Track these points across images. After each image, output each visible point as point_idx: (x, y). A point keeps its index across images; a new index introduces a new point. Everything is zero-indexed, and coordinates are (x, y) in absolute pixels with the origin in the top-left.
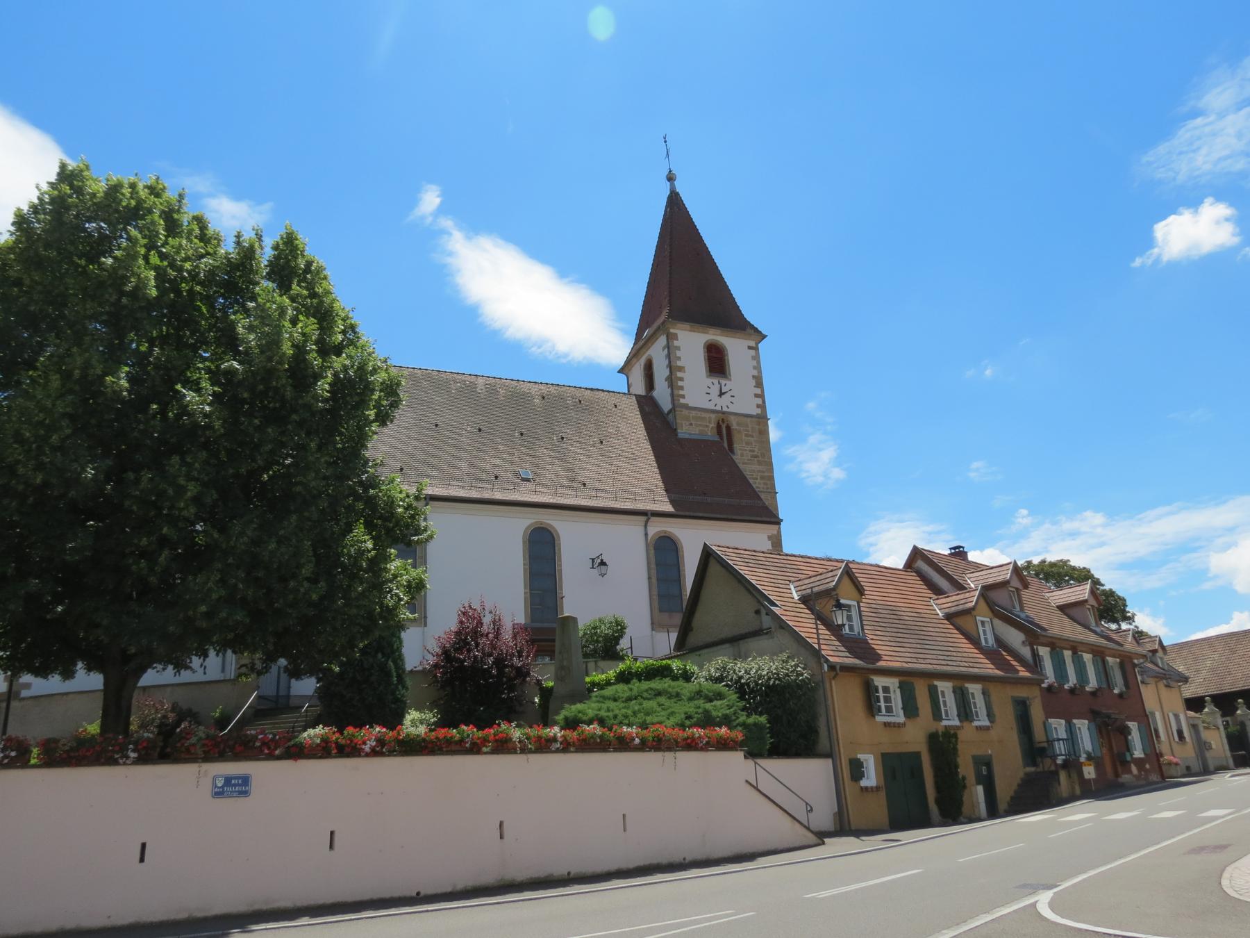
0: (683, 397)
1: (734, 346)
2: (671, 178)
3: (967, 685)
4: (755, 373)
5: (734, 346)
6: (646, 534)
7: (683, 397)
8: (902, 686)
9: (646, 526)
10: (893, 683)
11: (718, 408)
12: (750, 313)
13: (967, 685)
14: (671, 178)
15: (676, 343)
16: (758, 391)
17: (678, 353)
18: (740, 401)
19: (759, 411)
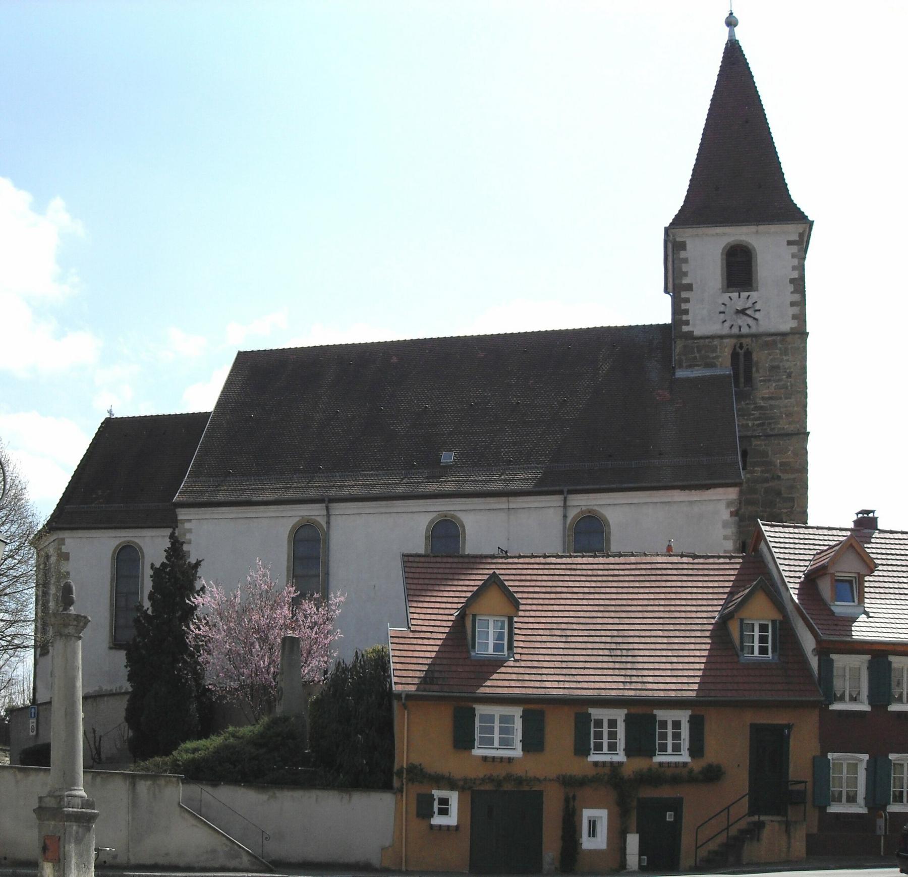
0: (687, 323)
1: (766, 243)
2: (731, 22)
3: (655, 712)
4: (795, 275)
5: (766, 243)
6: (565, 516)
7: (687, 323)
8: (871, 667)
9: (565, 507)
10: (861, 661)
11: (735, 330)
12: (800, 193)
13: (655, 712)
14: (731, 22)
15: (683, 254)
16: (796, 297)
17: (685, 268)
18: (771, 319)
19: (794, 324)
